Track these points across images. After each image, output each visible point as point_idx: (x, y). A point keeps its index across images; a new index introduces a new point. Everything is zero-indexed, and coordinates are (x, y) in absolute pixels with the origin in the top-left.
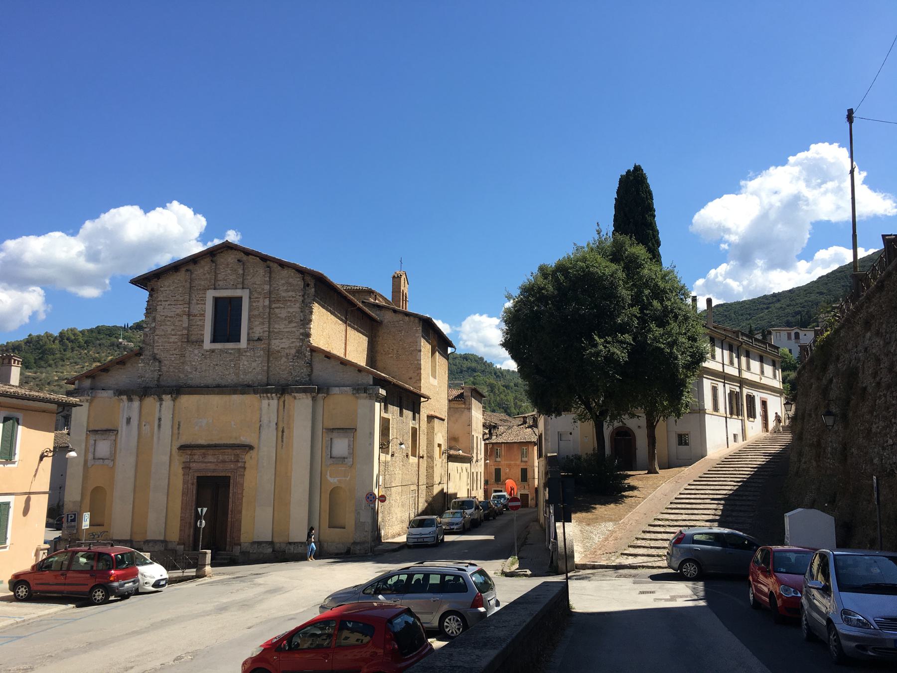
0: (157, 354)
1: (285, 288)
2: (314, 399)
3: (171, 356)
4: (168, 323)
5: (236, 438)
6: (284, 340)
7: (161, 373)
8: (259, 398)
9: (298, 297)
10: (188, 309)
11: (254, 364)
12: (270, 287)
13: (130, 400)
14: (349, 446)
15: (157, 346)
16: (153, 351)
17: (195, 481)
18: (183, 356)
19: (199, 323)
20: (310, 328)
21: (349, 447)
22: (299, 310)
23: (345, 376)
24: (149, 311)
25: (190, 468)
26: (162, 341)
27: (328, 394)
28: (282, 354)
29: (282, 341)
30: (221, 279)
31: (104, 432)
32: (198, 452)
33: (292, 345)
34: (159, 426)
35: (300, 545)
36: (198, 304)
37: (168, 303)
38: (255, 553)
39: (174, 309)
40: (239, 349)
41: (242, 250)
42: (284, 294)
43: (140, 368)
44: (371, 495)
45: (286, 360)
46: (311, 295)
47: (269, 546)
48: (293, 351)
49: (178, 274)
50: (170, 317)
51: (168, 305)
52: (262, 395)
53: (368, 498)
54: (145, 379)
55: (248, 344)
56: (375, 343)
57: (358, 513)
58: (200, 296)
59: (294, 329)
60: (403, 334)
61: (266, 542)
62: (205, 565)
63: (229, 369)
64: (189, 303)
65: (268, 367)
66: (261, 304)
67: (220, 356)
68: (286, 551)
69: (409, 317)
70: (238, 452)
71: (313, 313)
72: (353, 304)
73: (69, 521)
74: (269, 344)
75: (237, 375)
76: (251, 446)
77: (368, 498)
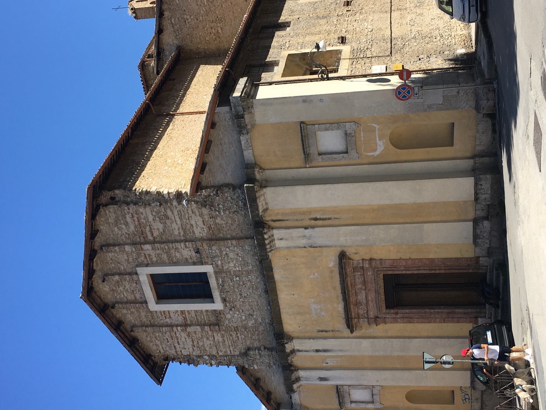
0: (240, 352)
1: (124, 227)
2: (265, 184)
3: (240, 338)
4: (201, 344)
5: (332, 272)
6: (193, 222)
7: (262, 347)
8: (273, 252)
9: (131, 211)
11: (231, 255)
13: (298, 379)
14: (326, 129)
16: (237, 356)
18: (236, 329)
19: (193, 315)
20: (168, 193)
22: (148, 209)
23: (226, 141)
24: (191, 361)
25: (377, 317)
27: (256, 164)
28: (212, 223)
29: (194, 225)
30: (133, 296)
31: (340, 396)
32: (354, 310)
34: (325, 351)
35: (480, 187)
36: (170, 317)
37: (176, 345)
38: (490, 241)
39: (183, 339)
40: (216, 273)
41: (87, 281)
42: (132, 228)
43: (259, 367)
44: (400, 93)
45: (218, 218)
46: (125, 194)
47: (480, 225)
48: (205, 211)
49: (139, 337)
50: (193, 342)
51: (179, 345)
52: (268, 250)
53: (404, 97)
54: (271, 363)
55: (206, 263)
56: (208, 52)
57: (430, 107)
58: (160, 315)
59: (176, 213)
60: (188, 17)
61: (475, 228)
63: (243, 282)
65: (233, 238)
67: (228, 291)
68: (488, 203)
69: (163, 11)
70: (349, 270)
71: (148, 190)
72: (163, 83)
74: (202, 239)
75: (248, 273)
76: (340, 254)
77: (404, 97)
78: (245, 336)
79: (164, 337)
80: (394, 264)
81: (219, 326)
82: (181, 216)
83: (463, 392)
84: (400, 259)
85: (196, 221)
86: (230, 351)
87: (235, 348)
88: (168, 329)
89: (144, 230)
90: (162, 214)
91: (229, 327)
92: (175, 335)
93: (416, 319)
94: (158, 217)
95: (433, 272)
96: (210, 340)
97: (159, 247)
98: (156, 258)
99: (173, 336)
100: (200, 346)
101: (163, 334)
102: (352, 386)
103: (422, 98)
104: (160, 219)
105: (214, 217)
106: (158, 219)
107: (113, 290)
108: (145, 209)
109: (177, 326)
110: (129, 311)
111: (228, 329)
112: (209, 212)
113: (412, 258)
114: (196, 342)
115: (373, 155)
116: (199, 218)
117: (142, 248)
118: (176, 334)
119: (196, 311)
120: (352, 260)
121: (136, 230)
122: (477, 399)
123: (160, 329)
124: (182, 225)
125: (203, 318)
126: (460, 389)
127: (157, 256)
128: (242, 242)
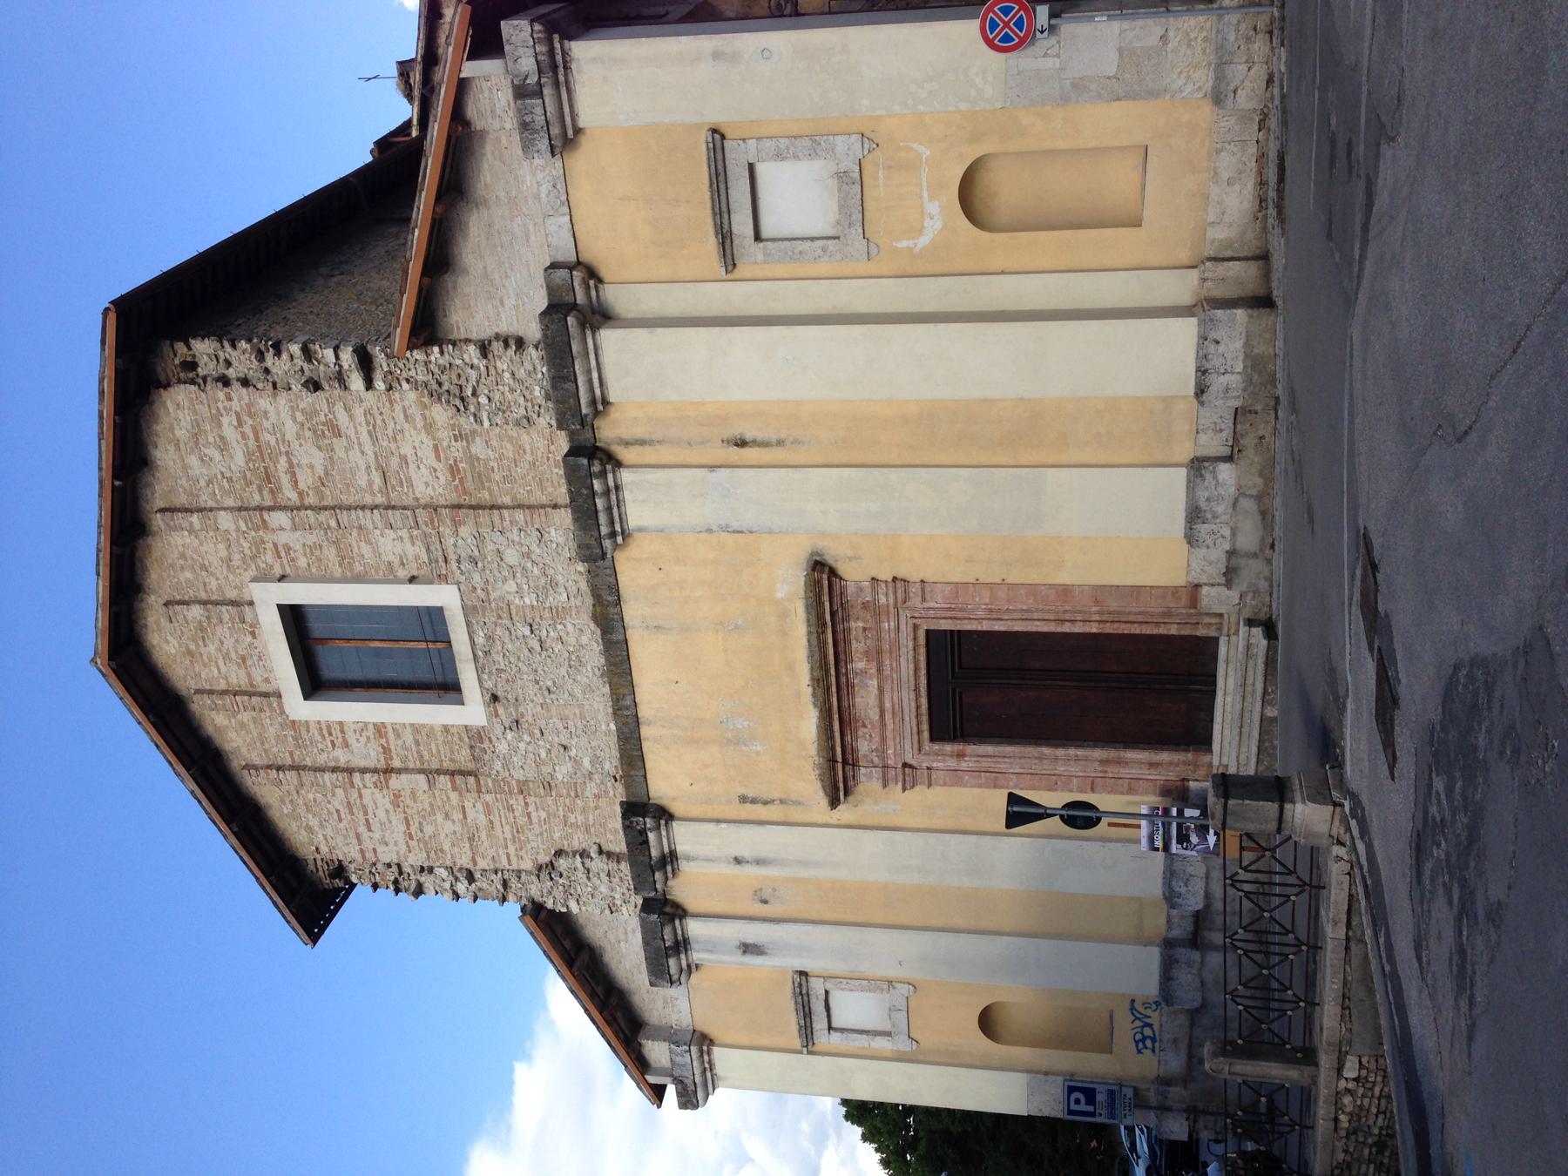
1: (216, 455)
3: (535, 820)
4: (429, 830)
5: (783, 616)
6: (407, 450)
9: (235, 405)
10: (368, 776)
11: (512, 557)
12: (225, 509)
15: (509, 861)
17: (948, 748)
19: (408, 737)
21: (784, 158)
26: (492, 847)
28: (459, 455)
29: (411, 458)
30: (242, 673)
33: (420, 423)
34: (759, 862)
36: (346, 745)
37: (362, 829)
38: (1234, 532)
39: (381, 814)
40: (468, 611)
42: (239, 459)
45: (478, 439)
47: (1208, 476)
48: (441, 414)
50: (408, 824)
51: (370, 830)
53: (1007, 38)
55: (443, 579)
57: (1079, 86)
58: (318, 738)
59: (358, 412)
62: (1250, 627)
64: (350, 771)
66: (294, 539)
68: (1237, 404)
73: (1091, 1108)
77: (1007, 38)
78: (549, 814)
79: (328, 806)
80: (957, 597)
81: (476, 776)
82: (374, 427)
83: (1139, 1016)
84: (976, 583)
85: (415, 448)
86: (508, 856)
87: (521, 849)
88: (337, 780)
89: (273, 468)
90: (323, 418)
91: (503, 780)
92: (358, 801)
93: (1013, 777)
94: (310, 429)
95: (1067, 628)
96: (453, 821)
97: (312, 520)
98: (305, 560)
99: (352, 802)
100: (426, 838)
101: (325, 796)
102: (833, 980)
103: (1058, 56)
104: (318, 435)
105: (466, 434)
106: (308, 434)
107: (190, 653)
108: (275, 402)
109: (364, 771)
110: (233, 720)
111: (501, 786)
112: (452, 418)
113: (1009, 581)
114: (417, 825)
115: (910, 249)
116: (423, 435)
117: (264, 521)
118: (361, 796)
119: (416, 729)
120: (841, 579)
121: (251, 465)
122: (1175, 1041)
123: (316, 777)
124: (376, 457)
125: (434, 751)
126: (1127, 1005)
127: (308, 550)
128: (539, 518)
